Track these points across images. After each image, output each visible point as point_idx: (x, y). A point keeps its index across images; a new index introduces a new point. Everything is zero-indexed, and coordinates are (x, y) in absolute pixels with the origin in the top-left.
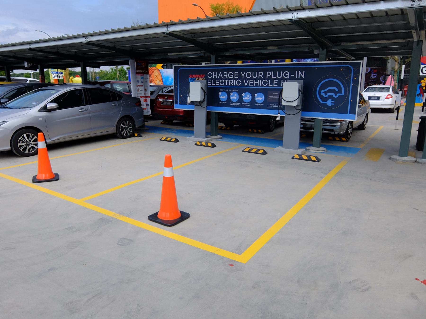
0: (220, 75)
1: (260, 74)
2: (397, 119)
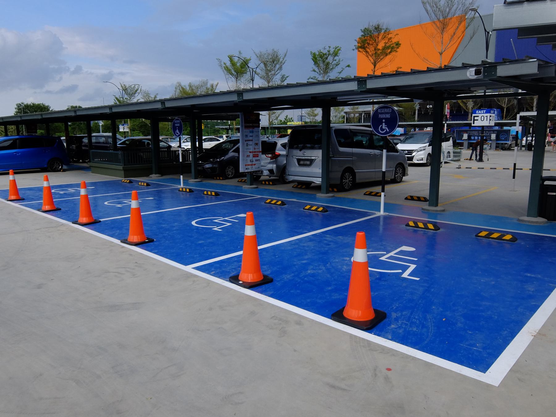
0: (472, 132)
1: (477, 132)
2: (514, 177)
